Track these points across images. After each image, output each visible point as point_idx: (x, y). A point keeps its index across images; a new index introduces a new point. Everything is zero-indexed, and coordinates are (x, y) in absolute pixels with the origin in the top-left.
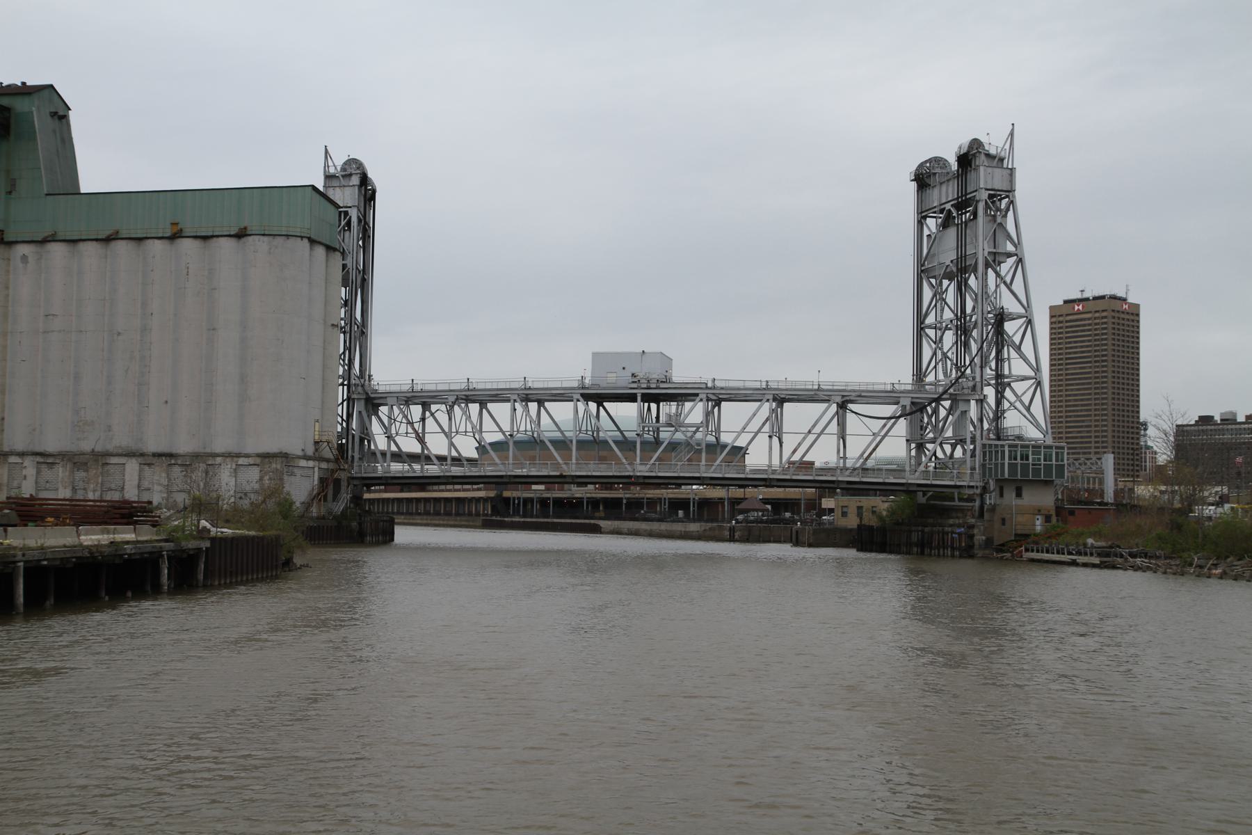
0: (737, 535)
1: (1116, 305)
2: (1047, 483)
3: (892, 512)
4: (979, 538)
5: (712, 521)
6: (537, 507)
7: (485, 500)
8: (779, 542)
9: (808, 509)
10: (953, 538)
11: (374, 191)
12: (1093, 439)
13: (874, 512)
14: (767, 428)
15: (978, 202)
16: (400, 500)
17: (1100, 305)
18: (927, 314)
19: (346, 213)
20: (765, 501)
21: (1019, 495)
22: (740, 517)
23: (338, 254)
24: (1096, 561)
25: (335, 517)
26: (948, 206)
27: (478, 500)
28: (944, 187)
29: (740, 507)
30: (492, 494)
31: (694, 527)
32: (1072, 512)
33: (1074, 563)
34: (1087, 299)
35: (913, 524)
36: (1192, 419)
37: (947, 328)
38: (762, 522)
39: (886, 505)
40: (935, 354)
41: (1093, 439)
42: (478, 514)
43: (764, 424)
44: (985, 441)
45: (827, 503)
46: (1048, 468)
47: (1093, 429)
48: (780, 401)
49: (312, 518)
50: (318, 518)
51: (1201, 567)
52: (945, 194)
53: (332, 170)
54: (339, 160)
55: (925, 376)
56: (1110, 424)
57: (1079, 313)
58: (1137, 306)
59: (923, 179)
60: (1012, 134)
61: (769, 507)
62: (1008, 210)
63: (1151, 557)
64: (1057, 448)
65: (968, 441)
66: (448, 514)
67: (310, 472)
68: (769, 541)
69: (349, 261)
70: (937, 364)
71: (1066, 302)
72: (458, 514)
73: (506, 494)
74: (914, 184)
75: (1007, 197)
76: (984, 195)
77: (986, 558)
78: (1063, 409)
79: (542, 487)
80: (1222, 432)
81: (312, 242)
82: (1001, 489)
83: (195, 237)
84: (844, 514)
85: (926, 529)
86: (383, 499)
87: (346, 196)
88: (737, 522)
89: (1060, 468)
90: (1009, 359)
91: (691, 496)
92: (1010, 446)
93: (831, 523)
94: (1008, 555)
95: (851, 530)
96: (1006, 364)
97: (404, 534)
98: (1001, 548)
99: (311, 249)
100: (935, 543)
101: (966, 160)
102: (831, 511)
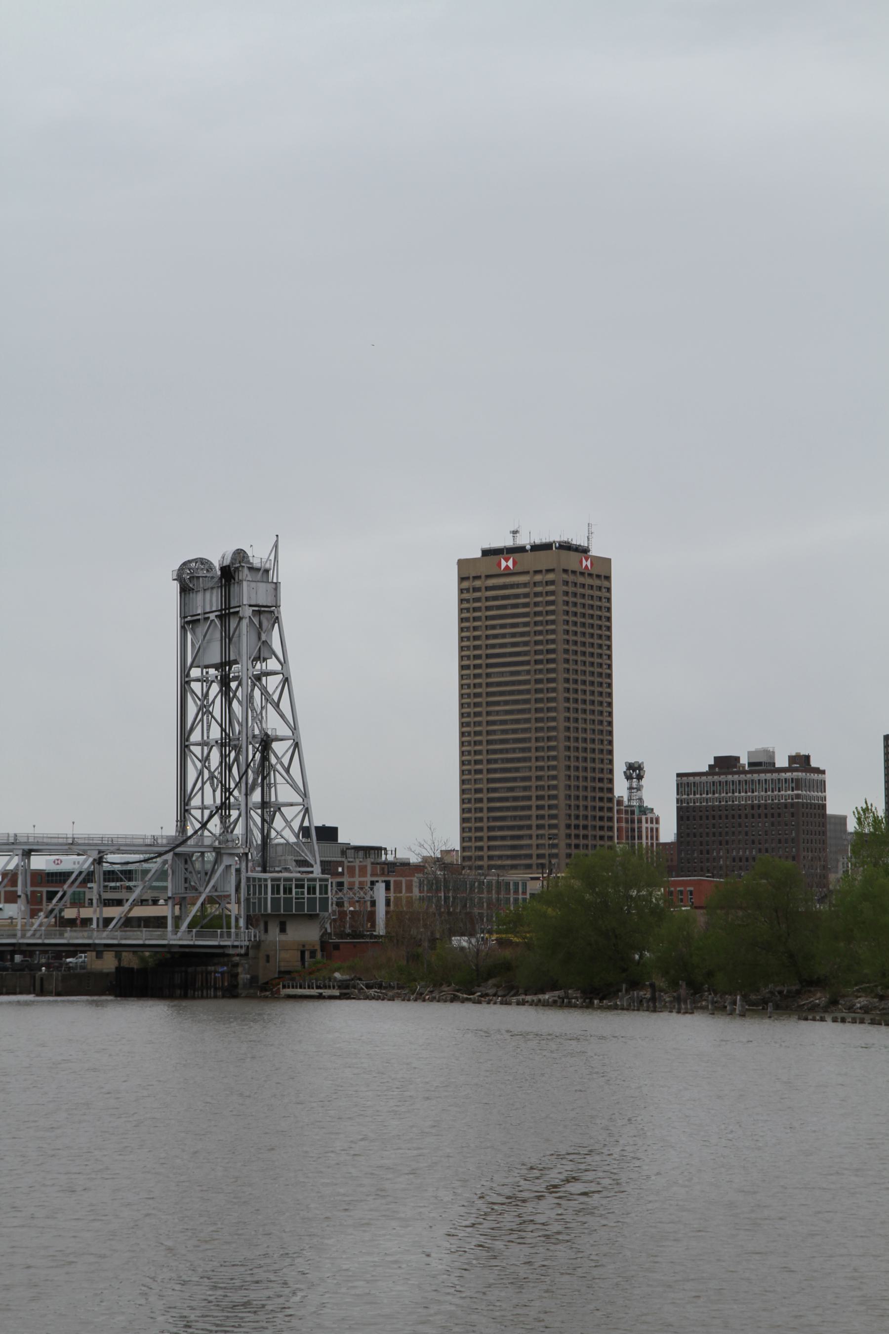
1: (571, 561)
2: (312, 917)
4: (244, 977)
10: (215, 978)
12: (534, 803)
15: (241, 619)
17: (544, 560)
18: (192, 729)
21: (283, 930)
24: (336, 992)
28: (208, 594)
32: (336, 947)
33: (320, 997)
34: (521, 549)
40: (201, 773)
41: (534, 803)
44: (250, 874)
47: (533, 783)
55: (190, 799)
56: (562, 774)
57: (508, 573)
58: (607, 562)
59: (189, 579)
60: (276, 546)
70: (203, 783)
71: (486, 553)
74: (176, 586)
77: (249, 997)
78: (483, 748)
80: (751, 786)
85: (190, 970)
89: (324, 902)
92: (273, 880)
95: (108, 974)
101: (228, 575)
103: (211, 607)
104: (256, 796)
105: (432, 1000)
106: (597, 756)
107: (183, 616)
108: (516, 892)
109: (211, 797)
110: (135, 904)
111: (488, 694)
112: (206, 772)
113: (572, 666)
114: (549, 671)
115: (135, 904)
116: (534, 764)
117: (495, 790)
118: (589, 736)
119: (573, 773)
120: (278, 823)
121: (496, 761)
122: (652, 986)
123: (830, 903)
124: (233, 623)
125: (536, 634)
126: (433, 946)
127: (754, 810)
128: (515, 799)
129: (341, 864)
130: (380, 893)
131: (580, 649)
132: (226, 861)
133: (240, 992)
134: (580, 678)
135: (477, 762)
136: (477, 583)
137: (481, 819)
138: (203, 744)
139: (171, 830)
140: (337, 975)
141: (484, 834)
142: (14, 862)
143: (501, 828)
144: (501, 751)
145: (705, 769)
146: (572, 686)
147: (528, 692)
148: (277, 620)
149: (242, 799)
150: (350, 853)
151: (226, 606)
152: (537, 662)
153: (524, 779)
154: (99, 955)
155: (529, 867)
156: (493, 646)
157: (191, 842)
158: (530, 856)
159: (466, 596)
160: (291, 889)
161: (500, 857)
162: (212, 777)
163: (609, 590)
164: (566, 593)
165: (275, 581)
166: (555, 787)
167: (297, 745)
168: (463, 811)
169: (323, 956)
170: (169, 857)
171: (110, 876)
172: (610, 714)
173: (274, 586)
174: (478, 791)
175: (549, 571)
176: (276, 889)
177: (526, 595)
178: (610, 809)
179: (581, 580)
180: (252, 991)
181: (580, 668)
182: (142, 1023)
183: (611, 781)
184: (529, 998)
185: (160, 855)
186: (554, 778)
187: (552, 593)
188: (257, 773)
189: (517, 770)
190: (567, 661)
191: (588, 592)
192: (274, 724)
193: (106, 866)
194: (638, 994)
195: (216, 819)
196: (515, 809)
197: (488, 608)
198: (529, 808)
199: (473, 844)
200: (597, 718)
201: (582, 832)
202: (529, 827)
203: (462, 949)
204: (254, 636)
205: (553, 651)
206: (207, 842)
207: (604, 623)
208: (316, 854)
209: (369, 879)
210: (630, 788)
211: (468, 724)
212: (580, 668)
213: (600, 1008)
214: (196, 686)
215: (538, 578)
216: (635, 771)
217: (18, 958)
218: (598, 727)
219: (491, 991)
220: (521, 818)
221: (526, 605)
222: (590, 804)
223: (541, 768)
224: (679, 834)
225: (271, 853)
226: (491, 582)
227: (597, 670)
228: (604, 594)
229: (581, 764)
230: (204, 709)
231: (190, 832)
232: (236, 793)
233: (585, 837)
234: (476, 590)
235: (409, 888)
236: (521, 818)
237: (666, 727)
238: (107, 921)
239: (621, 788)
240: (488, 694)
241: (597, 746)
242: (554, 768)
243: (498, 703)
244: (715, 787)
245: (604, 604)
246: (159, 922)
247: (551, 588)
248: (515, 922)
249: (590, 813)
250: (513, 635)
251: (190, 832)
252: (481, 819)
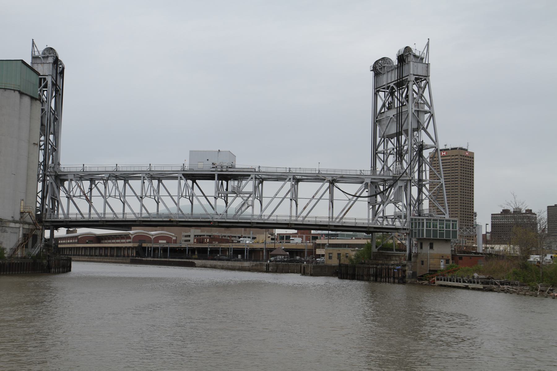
0: (270, 268)
1: (462, 153)
2: (447, 241)
3: (357, 257)
4: (409, 272)
5: (257, 261)
6: (160, 253)
7: (132, 248)
8: (294, 273)
9: (308, 255)
10: (394, 272)
11: (63, 69)
13: (347, 257)
14: (289, 196)
15: (409, 82)
16: (86, 248)
17: (455, 153)
18: (379, 145)
19: (45, 79)
20: (286, 250)
21: (431, 247)
22: (272, 259)
23: (38, 102)
24: (481, 286)
25: (32, 257)
26: (392, 85)
27: (129, 248)
28: (390, 74)
29: (272, 253)
30: (136, 245)
31: (246, 264)
32: (461, 258)
33: (467, 288)
34: (448, 149)
35: (371, 262)
36: (499, 211)
37: (390, 154)
38: (284, 261)
39: (354, 253)
40: (383, 168)
42: (128, 256)
43: (287, 194)
44: (412, 217)
45: (319, 252)
46: (448, 232)
48: (298, 181)
49: (17, 258)
50: (21, 258)
51: (542, 291)
52: (390, 78)
53: (37, 54)
54: (41, 48)
56: (459, 213)
58: (473, 153)
59: (379, 68)
60: (428, 44)
61: (288, 253)
62: (425, 87)
63: (512, 285)
64: (453, 221)
65: (403, 217)
66: (112, 256)
67: (17, 230)
68: (288, 272)
69: (46, 107)
72: (117, 256)
73: (144, 245)
74: (372, 73)
75: (425, 79)
76: (413, 78)
77: (412, 284)
79: (165, 242)
81: (21, 93)
82: (421, 244)
84: (330, 258)
85: (379, 267)
86: (77, 248)
87: (45, 69)
88: (271, 261)
90: (425, 171)
91: (245, 247)
92: (427, 220)
93: (323, 262)
94: (426, 282)
95: (334, 266)
96: (424, 173)
97: (77, 267)
98: (421, 278)
99: (21, 98)
100: (384, 275)
101: (402, 59)
102: (323, 255)
103: (391, 79)
112: (385, 167)
113: (462, 182)
127: (512, 224)
133: (407, 280)
134: (465, 186)
160: (437, 225)
163: (473, 161)
165: (427, 63)
169: (453, 263)
172: (473, 196)
173: (426, 65)
177: (449, 162)
179: (465, 158)
180: (413, 280)
186: (457, 214)
191: (467, 162)
194: (52, 234)
207: (472, 170)
215: (453, 157)
223: (453, 211)
228: (472, 162)
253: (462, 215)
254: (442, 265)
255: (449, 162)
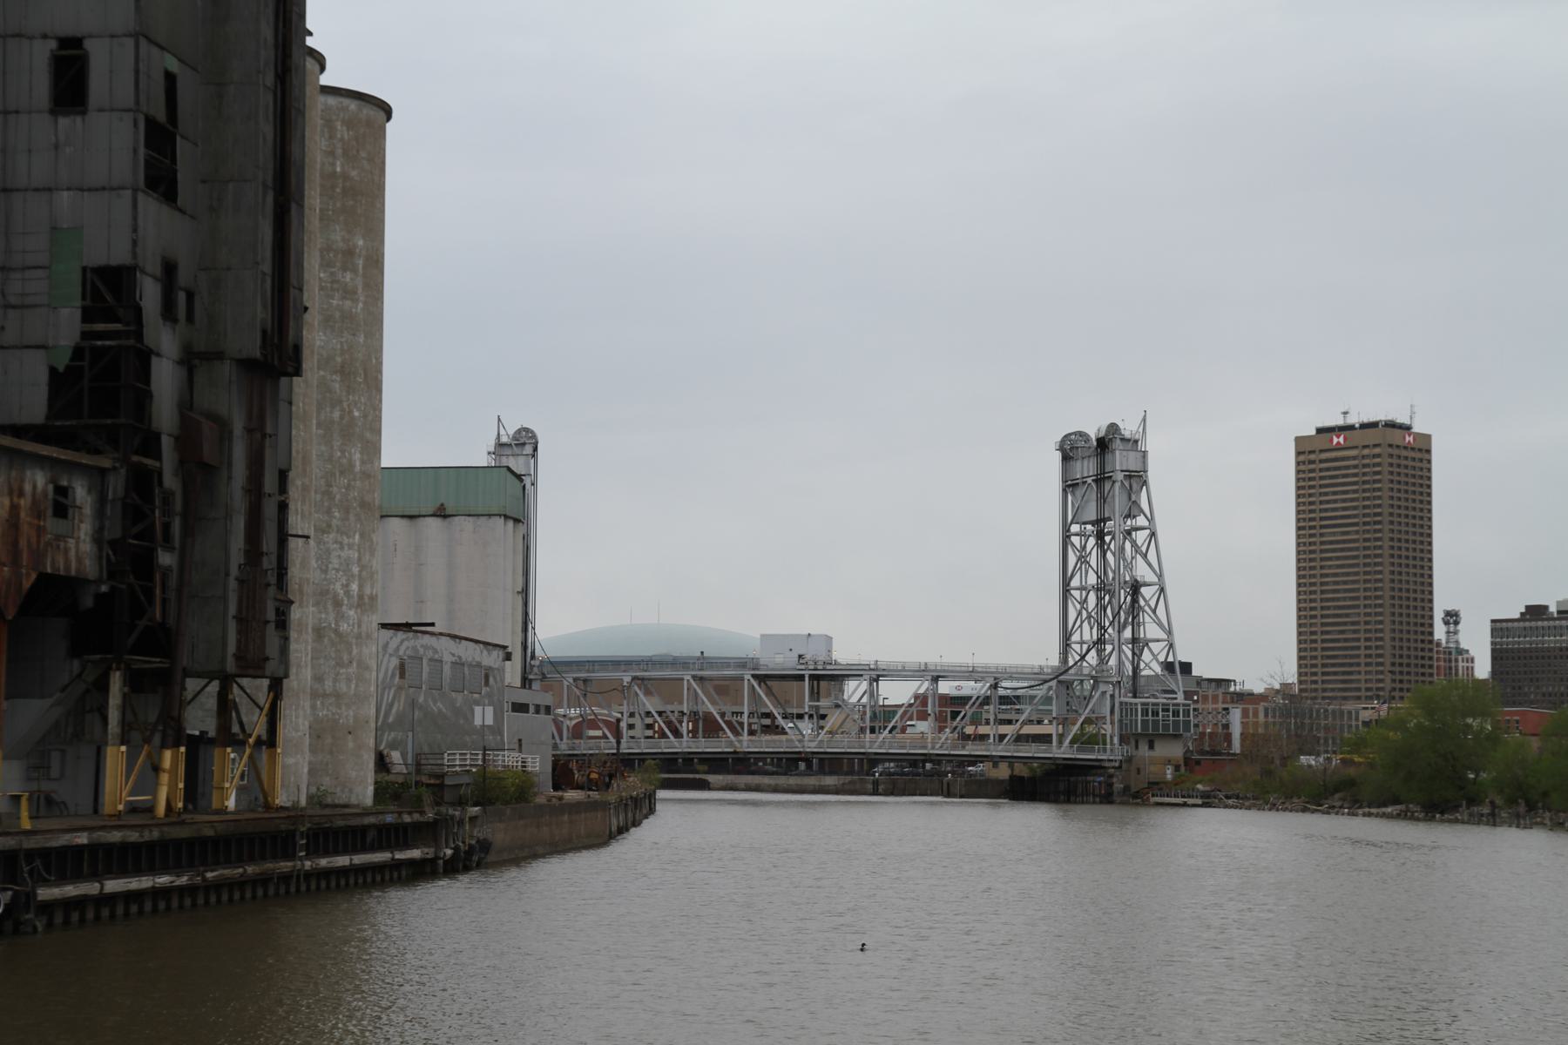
0: (881, 788)
1: (1395, 437)
2: (1176, 737)
4: (1118, 786)
12: (1362, 644)
17: (1371, 437)
21: (1151, 747)
24: (1199, 801)
32: (1198, 762)
33: (1185, 805)
34: (1351, 428)
40: (1080, 613)
53: (504, 439)
56: (1388, 619)
57: (1339, 448)
58: (1428, 438)
59: (1069, 450)
60: (1144, 420)
71: (1320, 431)
74: (1058, 455)
78: (1318, 596)
83: (403, 516)
89: (1187, 723)
100: (1079, 791)
101: (1103, 445)
104: (1128, 633)
105: (1285, 810)
106: (1419, 604)
107: (1065, 481)
108: (1350, 718)
109: (1088, 633)
110: (1024, 723)
111: (1322, 551)
113: (1396, 527)
114: (1376, 531)
115: (1024, 723)
116: (1362, 611)
117: (1327, 633)
118: (1412, 587)
119: (1397, 619)
120: (1146, 656)
121: (1328, 608)
122: (1492, 803)
123: (195, 784)
124: (1107, 486)
125: (1364, 501)
126: (1284, 765)
128: (1346, 640)
129: (1196, 693)
130: (1236, 716)
131: (1403, 512)
132: (1102, 688)
134: (1404, 537)
135: (1312, 609)
136: (1312, 457)
137: (1315, 658)
138: (1081, 588)
139: (1054, 661)
140: (1199, 786)
141: (1319, 670)
142: (924, 687)
143: (1333, 665)
144: (1333, 599)
145: (1517, 616)
146: (1396, 544)
147: (1357, 549)
148: (1145, 483)
149: (1115, 636)
150: (1205, 684)
151: (1101, 472)
152: (1365, 524)
153: (1353, 623)
154: (995, 765)
155: (1359, 698)
156: (1326, 510)
157: (1072, 671)
158: (1359, 689)
159: (1302, 467)
161: (1333, 690)
162: (1089, 617)
163: (1429, 461)
164: (1391, 465)
166: (1381, 631)
167: (1162, 590)
168: (1300, 650)
170: (1053, 683)
171: (1004, 700)
174: (1313, 633)
175: (1375, 446)
176: (1145, 712)
177: (1355, 467)
178: (1431, 650)
179: (1404, 453)
181: (1403, 528)
182: (1032, 823)
183: (1431, 625)
184: (1374, 810)
185: (1046, 681)
186: (1381, 622)
187: (1379, 465)
188: (1127, 614)
189: (1347, 615)
190: (1392, 523)
192: (1142, 571)
193: (1001, 692)
195: (1093, 653)
196: (1346, 648)
197: (1321, 478)
198: (1358, 648)
199: (1309, 678)
200: (1419, 571)
201: (1405, 669)
202: (1358, 665)
203: (1310, 766)
204: (1125, 497)
205: (1379, 514)
206: (1086, 671)
207: (1425, 490)
208: (1178, 684)
209: (1220, 706)
210: (1448, 632)
211: (1304, 577)
212: (1403, 528)
213: (1442, 821)
214: (1076, 540)
215: (1366, 452)
216: (1452, 618)
217: (928, 766)
218: (1419, 580)
219: (1338, 804)
220: (1352, 657)
221: (1355, 475)
222: (1412, 645)
223: (1369, 614)
224: (1494, 672)
225: (1142, 682)
226: (1324, 456)
227: (1418, 530)
229: (1404, 611)
230: (1083, 559)
231: (1071, 663)
232: (1110, 630)
233: (1409, 673)
234: (1311, 462)
235: (1256, 714)
236: (1352, 657)
237: (1479, 581)
238: (1002, 737)
239: (1440, 632)
240: (1322, 551)
241: (1419, 596)
242: (1381, 614)
243: (1330, 559)
244: (1526, 632)
245: (1425, 473)
246: (1045, 739)
247: (1377, 460)
248: (1358, 745)
249: (1413, 653)
250: (1344, 501)
251: (1071, 663)
252: (1315, 658)
253: (1397, 627)
254: (1169, 774)
255: (1355, 467)
